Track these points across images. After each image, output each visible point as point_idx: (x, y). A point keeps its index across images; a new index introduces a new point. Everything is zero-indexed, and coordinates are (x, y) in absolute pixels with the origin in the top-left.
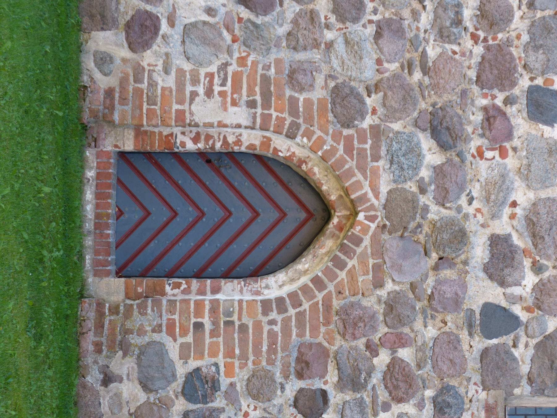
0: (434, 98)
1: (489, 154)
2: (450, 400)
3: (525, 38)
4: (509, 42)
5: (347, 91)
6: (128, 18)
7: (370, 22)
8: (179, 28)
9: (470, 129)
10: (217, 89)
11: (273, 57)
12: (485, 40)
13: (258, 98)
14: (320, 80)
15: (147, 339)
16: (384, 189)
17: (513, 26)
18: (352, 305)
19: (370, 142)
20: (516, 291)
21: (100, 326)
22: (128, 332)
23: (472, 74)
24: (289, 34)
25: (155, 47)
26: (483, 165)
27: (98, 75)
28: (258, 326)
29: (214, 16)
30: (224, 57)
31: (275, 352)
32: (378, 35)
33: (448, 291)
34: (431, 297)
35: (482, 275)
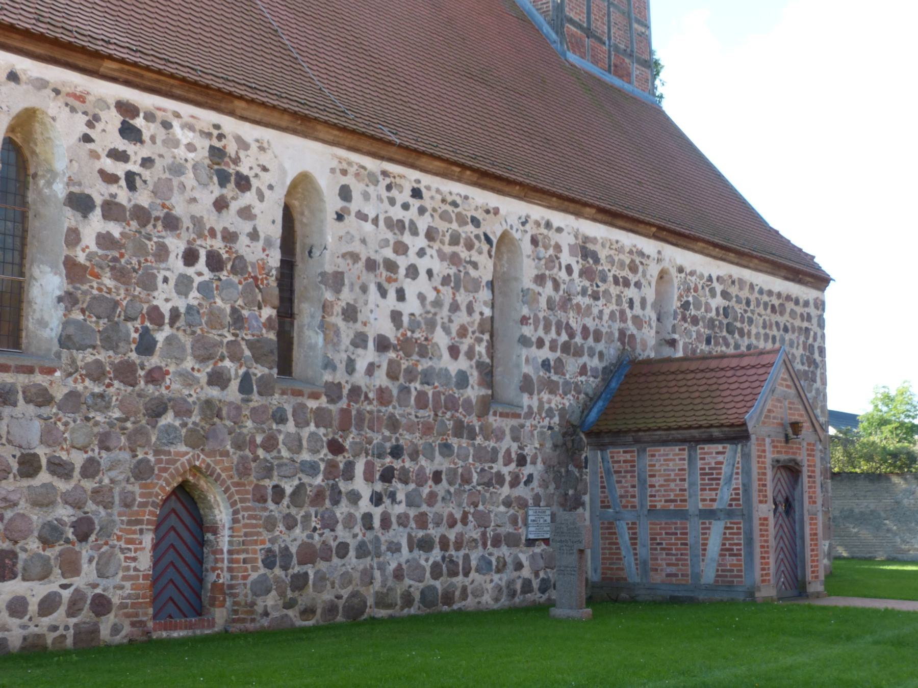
0: (141, 415)
1: (168, 382)
2: (279, 415)
3: (111, 353)
4: (111, 364)
5: (137, 470)
6: (93, 615)
7: (99, 453)
8: (99, 580)
9: (157, 393)
10: (133, 554)
11: (116, 518)
12: (111, 379)
13: (138, 527)
14: (129, 488)
15: (249, 592)
16: (183, 448)
17: (103, 360)
18: (237, 470)
19: (162, 457)
20: (233, 372)
21: (243, 620)
22: (246, 604)
23: (130, 389)
24: (105, 507)
25: (110, 596)
26: (173, 386)
27: (123, 633)
28: (245, 526)
29: (94, 557)
30: (117, 551)
31: (256, 515)
32: (108, 449)
33: (233, 413)
34: (235, 423)
35: (225, 392)
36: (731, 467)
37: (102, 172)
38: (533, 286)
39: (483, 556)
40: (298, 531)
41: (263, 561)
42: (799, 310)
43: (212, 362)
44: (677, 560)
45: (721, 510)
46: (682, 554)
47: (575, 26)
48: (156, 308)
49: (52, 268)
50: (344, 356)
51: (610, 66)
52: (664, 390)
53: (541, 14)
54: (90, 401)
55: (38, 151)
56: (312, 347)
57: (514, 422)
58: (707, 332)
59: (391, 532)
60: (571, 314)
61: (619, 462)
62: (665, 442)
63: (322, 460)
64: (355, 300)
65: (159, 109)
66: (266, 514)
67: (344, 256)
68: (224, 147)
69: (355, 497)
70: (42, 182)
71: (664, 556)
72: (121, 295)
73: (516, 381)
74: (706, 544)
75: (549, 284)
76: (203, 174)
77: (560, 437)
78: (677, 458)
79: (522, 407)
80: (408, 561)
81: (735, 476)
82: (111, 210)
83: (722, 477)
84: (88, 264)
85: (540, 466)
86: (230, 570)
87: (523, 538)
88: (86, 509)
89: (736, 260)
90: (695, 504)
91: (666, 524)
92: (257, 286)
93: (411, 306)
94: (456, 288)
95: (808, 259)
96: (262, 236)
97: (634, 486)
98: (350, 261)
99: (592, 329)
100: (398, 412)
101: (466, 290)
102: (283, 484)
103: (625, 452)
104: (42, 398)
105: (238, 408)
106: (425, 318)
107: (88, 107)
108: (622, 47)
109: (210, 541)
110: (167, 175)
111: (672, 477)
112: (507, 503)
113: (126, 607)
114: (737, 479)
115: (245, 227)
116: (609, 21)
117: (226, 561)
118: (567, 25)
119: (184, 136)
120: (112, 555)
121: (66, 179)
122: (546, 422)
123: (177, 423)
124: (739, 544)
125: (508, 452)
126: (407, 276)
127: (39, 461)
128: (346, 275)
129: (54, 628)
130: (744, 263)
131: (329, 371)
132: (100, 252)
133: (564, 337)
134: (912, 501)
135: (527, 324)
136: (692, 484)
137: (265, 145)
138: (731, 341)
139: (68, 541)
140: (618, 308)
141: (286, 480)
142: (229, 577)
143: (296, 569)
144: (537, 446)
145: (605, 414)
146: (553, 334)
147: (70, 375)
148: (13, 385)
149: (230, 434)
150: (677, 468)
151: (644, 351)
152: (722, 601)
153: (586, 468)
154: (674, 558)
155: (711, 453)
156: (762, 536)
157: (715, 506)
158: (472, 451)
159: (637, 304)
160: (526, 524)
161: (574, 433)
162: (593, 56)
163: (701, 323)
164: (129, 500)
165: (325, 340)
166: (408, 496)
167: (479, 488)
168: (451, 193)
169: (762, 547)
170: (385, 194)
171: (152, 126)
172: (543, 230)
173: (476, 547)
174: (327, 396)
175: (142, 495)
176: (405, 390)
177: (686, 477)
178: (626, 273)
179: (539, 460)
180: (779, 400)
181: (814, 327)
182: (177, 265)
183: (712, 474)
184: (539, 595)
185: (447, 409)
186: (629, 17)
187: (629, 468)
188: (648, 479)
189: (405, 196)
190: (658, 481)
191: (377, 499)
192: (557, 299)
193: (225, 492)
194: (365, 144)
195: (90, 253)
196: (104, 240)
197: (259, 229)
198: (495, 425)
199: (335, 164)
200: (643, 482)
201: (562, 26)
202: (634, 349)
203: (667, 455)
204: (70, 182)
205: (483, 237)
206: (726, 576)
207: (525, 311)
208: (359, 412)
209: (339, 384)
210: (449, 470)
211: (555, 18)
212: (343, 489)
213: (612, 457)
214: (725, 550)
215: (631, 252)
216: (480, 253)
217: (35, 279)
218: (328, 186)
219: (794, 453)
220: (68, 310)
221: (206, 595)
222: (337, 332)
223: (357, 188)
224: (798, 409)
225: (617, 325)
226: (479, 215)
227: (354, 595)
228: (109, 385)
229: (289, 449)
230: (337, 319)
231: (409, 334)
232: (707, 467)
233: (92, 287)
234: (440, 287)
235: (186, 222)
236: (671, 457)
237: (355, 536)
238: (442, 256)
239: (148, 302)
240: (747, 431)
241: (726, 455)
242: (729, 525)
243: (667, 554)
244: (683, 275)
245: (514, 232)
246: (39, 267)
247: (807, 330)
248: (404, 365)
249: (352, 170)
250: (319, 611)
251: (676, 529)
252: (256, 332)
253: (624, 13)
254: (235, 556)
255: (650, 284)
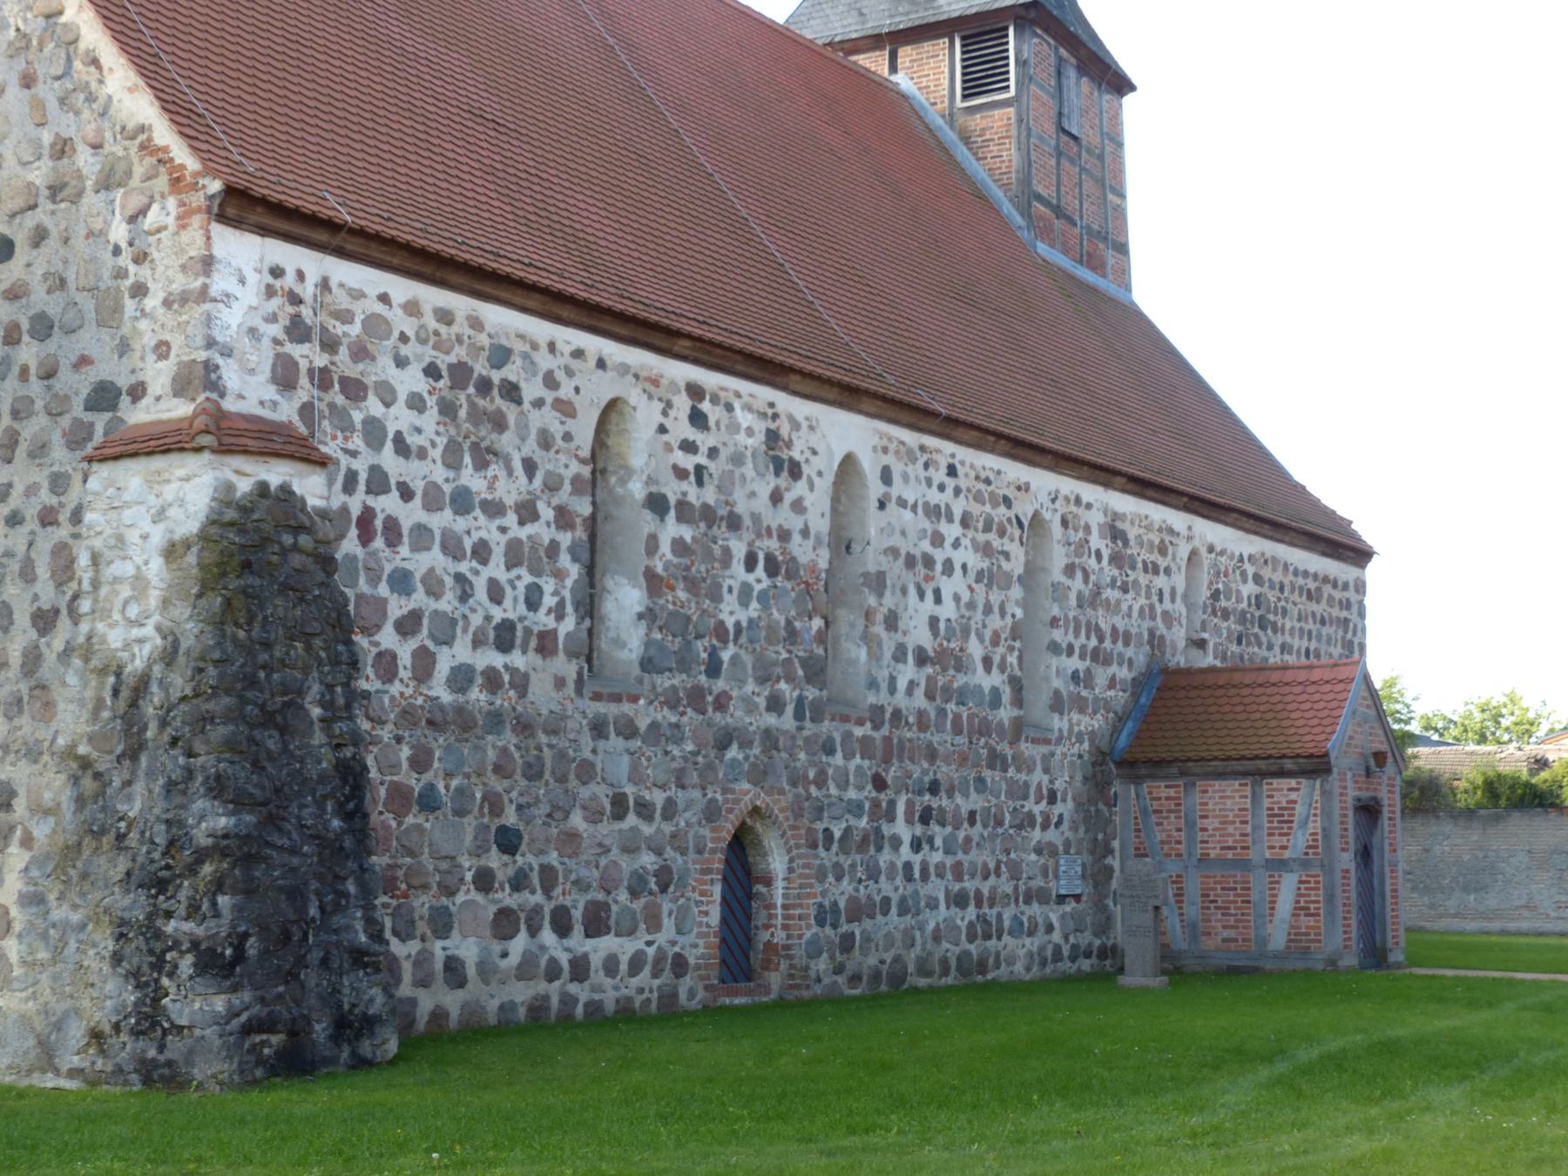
3: (684, 676)
8: (678, 938)
9: (723, 722)
13: (709, 877)
16: (746, 786)
18: (793, 811)
20: (788, 696)
21: (798, 987)
27: (698, 998)
30: (692, 904)
32: (683, 787)
35: (781, 719)
36: (1307, 807)
37: (675, 467)
38: (1063, 579)
39: (1015, 915)
40: (845, 882)
41: (815, 917)
42: (1337, 595)
43: (770, 683)
44: (1236, 921)
45: (1294, 860)
46: (1243, 914)
47: (1042, 204)
48: (722, 623)
49: (629, 579)
50: (885, 673)
51: (1082, 256)
52: (1213, 709)
53: (1000, 187)
54: (668, 733)
55: (609, 442)
56: (853, 662)
57: (1044, 749)
58: (1239, 628)
59: (930, 885)
60: (1101, 612)
61: (1160, 799)
62: (1220, 775)
63: (867, 798)
64: (897, 605)
65: (722, 389)
66: (818, 862)
67: (886, 552)
68: (778, 428)
69: (896, 842)
70: (613, 480)
71: (1220, 917)
72: (692, 611)
73: (1045, 697)
74: (1275, 902)
75: (1079, 575)
76: (761, 459)
77: (1090, 767)
78: (1237, 795)
79: (1051, 730)
80: (945, 920)
81: (1312, 818)
82: (685, 511)
83: (1295, 819)
84: (664, 574)
85: (1070, 804)
86: (785, 927)
87: (1054, 893)
88: (666, 856)
89: (1270, 533)
90: (1261, 852)
91: (1222, 876)
92: (809, 593)
93: (947, 611)
94: (989, 586)
95: (1343, 525)
96: (813, 532)
97: (1179, 830)
98: (891, 558)
99: (1121, 630)
100: (936, 739)
101: (1000, 588)
102: (832, 827)
103: (1167, 787)
104: (628, 730)
105: (793, 738)
106: (960, 624)
107: (661, 392)
108: (1096, 227)
109: (762, 895)
110: (730, 467)
111: (1231, 818)
112: (1038, 851)
113: (699, 969)
114: (1315, 821)
115: (796, 523)
116: (1081, 194)
117: (780, 918)
118: (1035, 203)
119: (744, 419)
120: (688, 908)
121: (644, 478)
122: (1075, 750)
123: (740, 757)
124: (1318, 902)
125: (1039, 786)
126: (943, 573)
127: (627, 802)
128: (888, 576)
129: (641, 991)
130: (1279, 536)
131: (873, 691)
132: (676, 560)
133: (1094, 642)
134: (1447, 848)
135: (1057, 627)
136: (1256, 828)
137: (814, 424)
138: (1264, 640)
139: (651, 893)
140: (1148, 602)
141: (835, 822)
142: (785, 937)
143: (845, 928)
144: (1067, 779)
145: (1138, 737)
146: (1083, 639)
147: (651, 702)
148: (606, 715)
149: (786, 768)
150: (1236, 807)
151: (1173, 656)
152: (1294, 971)
153: (1115, 806)
154: (1232, 918)
155: (1282, 790)
156: (1344, 891)
157: (1287, 854)
158: (1004, 787)
159: (1167, 596)
160: (1056, 877)
161: (1103, 763)
162: (1063, 244)
163: (1232, 617)
164: (701, 846)
165: (869, 654)
166: (945, 841)
167: (1011, 831)
168: (984, 468)
169: (1345, 905)
170: (922, 474)
171: (717, 409)
172: (1074, 509)
173: (1008, 904)
174: (872, 721)
175: (713, 840)
176: (942, 712)
177: (1249, 818)
178: (1155, 557)
179: (1070, 796)
180: (1359, 725)
181: (1354, 617)
182: (738, 568)
183: (1283, 815)
184: (1069, 964)
185: (981, 734)
186: (1103, 185)
187: (1173, 807)
188: (1199, 821)
189: (940, 475)
190: (1211, 824)
191: (916, 846)
192: (1087, 593)
193: (782, 836)
194: (905, 416)
195: (667, 562)
196: (679, 546)
197: (810, 524)
198: (1027, 753)
199: (875, 440)
200: (1191, 825)
201: (1030, 205)
202: (1163, 653)
203: (1224, 791)
204: (650, 480)
205: (1014, 520)
206: (1300, 941)
207: (1056, 611)
208: (901, 741)
209: (882, 706)
210: (984, 808)
211: (1020, 194)
212: (886, 833)
213: (1150, 793)
214: (1299, 909)
215: (1160, 530)
216: (1012, 540)
217: (609, 592)
218: (869, 465)
219: (1375, 790)
220: (650, 629)
221: (756, 959)
222: (880, 645)
223: (897, 469)
224: (1379, 736)
225: (1147, 624)
226: (1011, 493)
227: (897, 959)
228: (683, 714)
229: (838, 786)
230: (879, 629)
231: (945, 643)
232: (1276, 806)
233: (667, 601)
234: (974, 585)
235: (747, 521)
236: (1229, 793)
237: (896, 889)
238: (976, 547)
239: (714, 616)
240: (1329, 763)
241: (1301, 792)
242: (1304, 878)
243: (1223, 914)
244: (1213, 555)
245: (1044, 511)
246: (613, 578)
247: (1346, 621)
248: (941, 681)
249: (893, 447)
250: (865, 978)
251: (1235, 882)
252: (808, 648)
253: (1097, 181)
254: (791, 912)
255: (1179, 569)
